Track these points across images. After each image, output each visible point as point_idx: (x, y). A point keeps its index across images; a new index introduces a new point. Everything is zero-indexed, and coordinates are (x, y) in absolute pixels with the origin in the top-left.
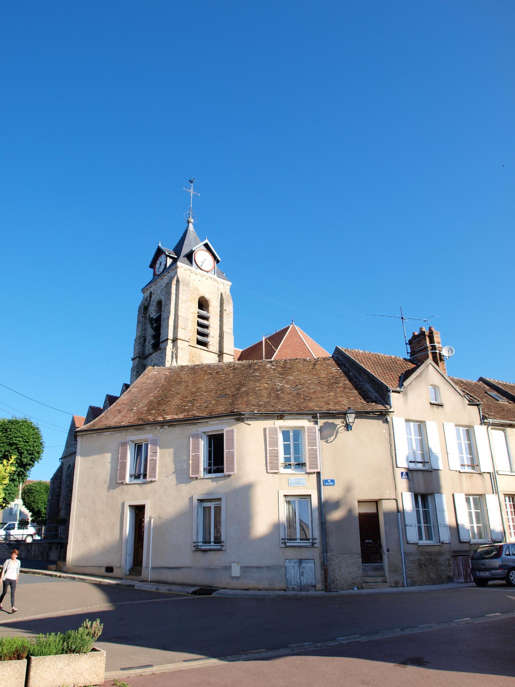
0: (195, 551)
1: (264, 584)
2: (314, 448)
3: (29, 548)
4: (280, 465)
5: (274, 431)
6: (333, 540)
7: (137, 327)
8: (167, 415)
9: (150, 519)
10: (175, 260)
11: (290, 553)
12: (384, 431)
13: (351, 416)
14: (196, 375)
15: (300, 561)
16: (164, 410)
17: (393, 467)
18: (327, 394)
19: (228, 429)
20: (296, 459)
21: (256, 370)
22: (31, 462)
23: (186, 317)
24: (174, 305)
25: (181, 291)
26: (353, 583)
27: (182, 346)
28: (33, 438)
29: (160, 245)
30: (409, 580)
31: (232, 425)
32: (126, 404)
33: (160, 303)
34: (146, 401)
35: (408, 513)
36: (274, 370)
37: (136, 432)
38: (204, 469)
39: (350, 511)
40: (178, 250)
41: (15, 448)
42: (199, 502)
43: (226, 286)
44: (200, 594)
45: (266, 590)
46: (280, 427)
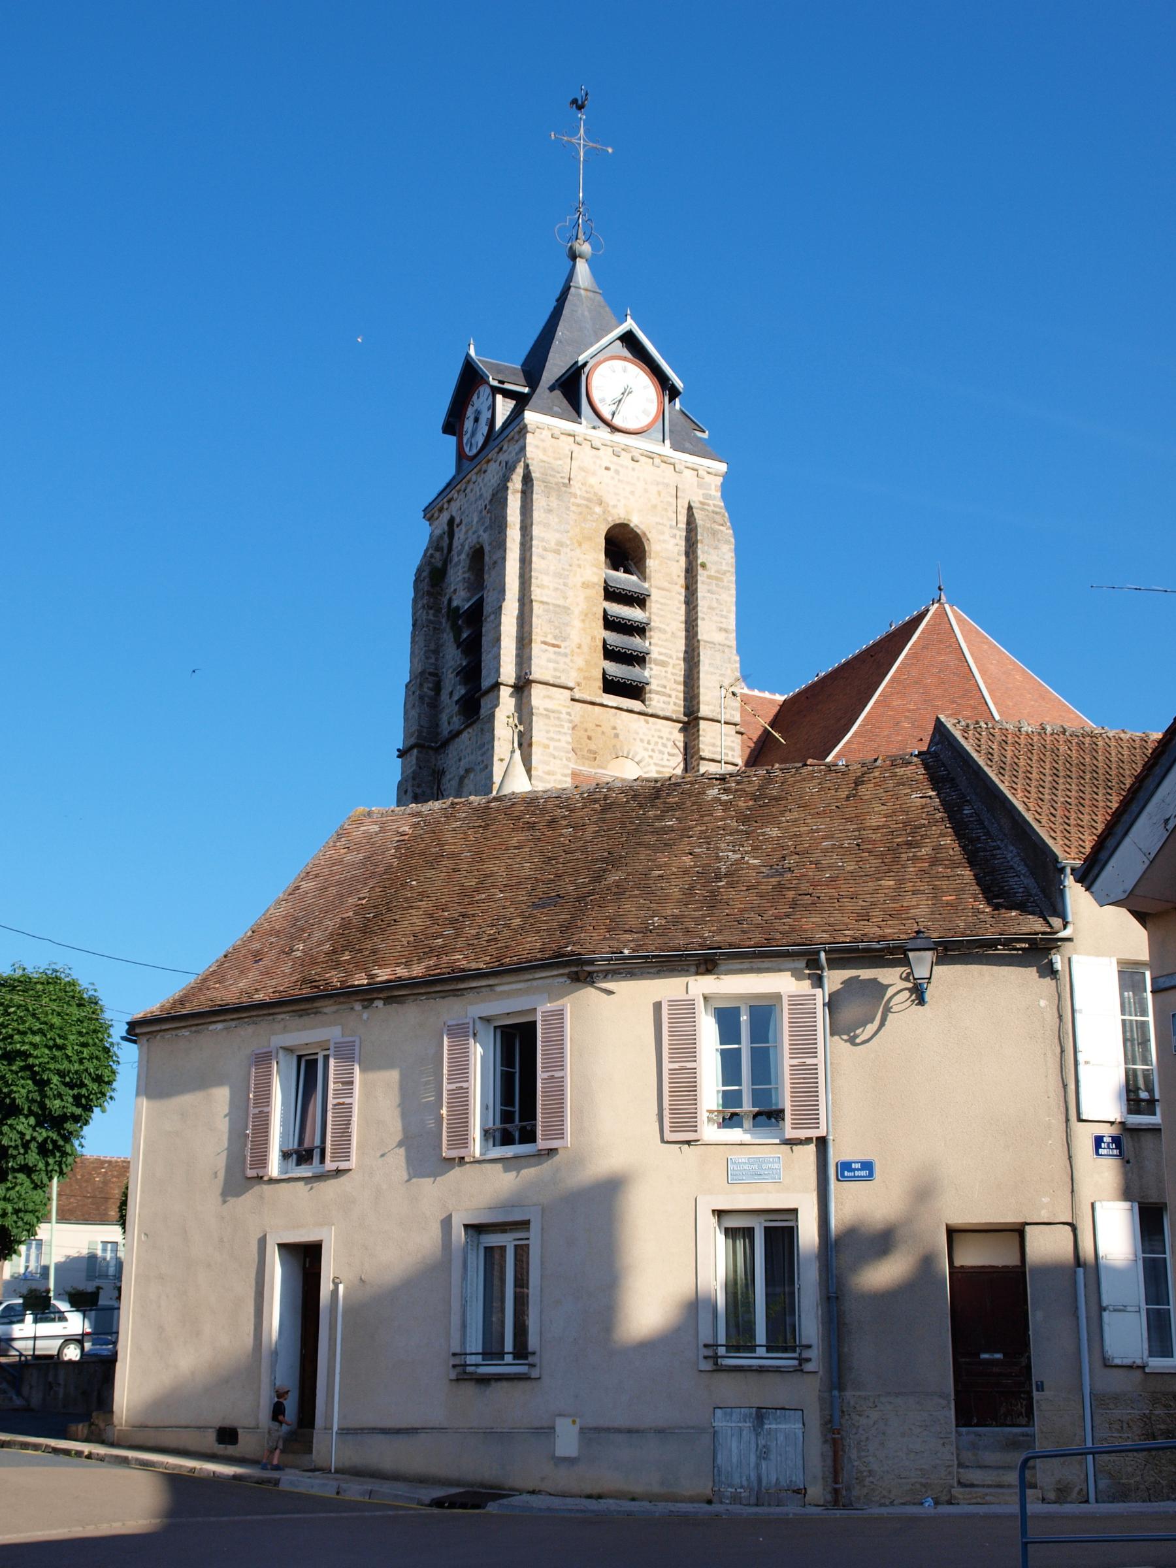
0: (458, 1380)
1: (647, 1481)
2: (809, 1061)
3: (51, 1379)
4: (703, 1116)
5: (685, 1010)
6: (864, 1352)
7: (413, 642)
8: (380, 967)
9: (336, 1285)
10: (522, 401)
11: (729, 1389)
12: (1043, 1003)
13: (919, 959)
14: (489, 834)
15: (760, 1415)
16: (374, 952)
17: (1067, 1120)
18: (871, 885)
19: (549, 1006)
20: (757, 1096)
21: (670, 808)
22: (78, 1111)
23: (561, 602)
24: (517, 565)
25: (538, 515)
26: (924, 1485)
27: (550, 705)
28: (80, 1033)
29: (472, 352)
30: (1103, 1483)
31: (561, 996)
32: (277, 933)
33: (478, 555)
34: (331, 923)
35: (1114, 1270)
36: (726, 806)
37: (297, 1022)
38: (486, 1133)
39: (927, 1262)
40: (533, 370)
41: (22, 1069)
42: (470, 1231)
43: (708, 479)
44: (464, 1506)
45: (652, 1498)
46: (706, 998)
